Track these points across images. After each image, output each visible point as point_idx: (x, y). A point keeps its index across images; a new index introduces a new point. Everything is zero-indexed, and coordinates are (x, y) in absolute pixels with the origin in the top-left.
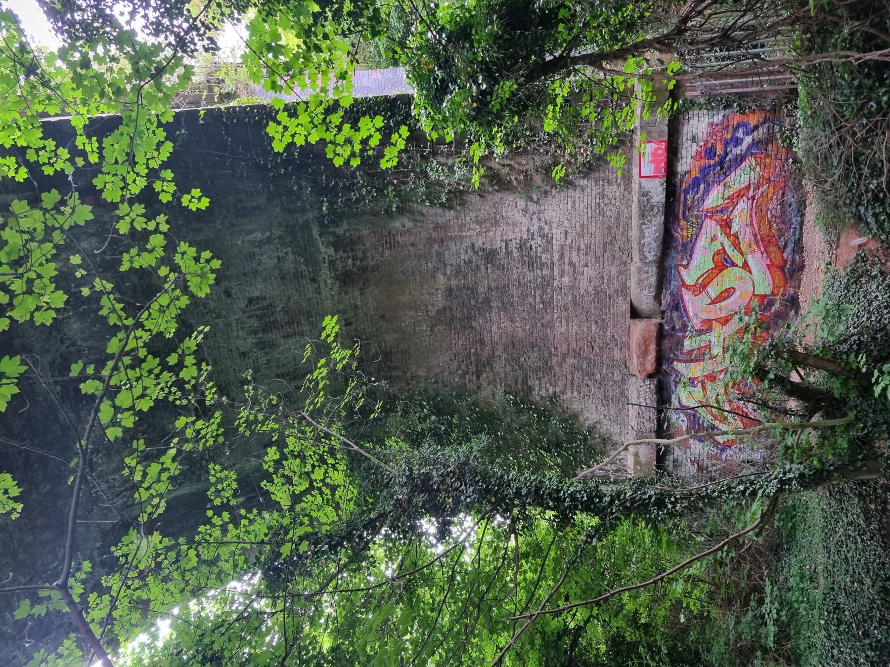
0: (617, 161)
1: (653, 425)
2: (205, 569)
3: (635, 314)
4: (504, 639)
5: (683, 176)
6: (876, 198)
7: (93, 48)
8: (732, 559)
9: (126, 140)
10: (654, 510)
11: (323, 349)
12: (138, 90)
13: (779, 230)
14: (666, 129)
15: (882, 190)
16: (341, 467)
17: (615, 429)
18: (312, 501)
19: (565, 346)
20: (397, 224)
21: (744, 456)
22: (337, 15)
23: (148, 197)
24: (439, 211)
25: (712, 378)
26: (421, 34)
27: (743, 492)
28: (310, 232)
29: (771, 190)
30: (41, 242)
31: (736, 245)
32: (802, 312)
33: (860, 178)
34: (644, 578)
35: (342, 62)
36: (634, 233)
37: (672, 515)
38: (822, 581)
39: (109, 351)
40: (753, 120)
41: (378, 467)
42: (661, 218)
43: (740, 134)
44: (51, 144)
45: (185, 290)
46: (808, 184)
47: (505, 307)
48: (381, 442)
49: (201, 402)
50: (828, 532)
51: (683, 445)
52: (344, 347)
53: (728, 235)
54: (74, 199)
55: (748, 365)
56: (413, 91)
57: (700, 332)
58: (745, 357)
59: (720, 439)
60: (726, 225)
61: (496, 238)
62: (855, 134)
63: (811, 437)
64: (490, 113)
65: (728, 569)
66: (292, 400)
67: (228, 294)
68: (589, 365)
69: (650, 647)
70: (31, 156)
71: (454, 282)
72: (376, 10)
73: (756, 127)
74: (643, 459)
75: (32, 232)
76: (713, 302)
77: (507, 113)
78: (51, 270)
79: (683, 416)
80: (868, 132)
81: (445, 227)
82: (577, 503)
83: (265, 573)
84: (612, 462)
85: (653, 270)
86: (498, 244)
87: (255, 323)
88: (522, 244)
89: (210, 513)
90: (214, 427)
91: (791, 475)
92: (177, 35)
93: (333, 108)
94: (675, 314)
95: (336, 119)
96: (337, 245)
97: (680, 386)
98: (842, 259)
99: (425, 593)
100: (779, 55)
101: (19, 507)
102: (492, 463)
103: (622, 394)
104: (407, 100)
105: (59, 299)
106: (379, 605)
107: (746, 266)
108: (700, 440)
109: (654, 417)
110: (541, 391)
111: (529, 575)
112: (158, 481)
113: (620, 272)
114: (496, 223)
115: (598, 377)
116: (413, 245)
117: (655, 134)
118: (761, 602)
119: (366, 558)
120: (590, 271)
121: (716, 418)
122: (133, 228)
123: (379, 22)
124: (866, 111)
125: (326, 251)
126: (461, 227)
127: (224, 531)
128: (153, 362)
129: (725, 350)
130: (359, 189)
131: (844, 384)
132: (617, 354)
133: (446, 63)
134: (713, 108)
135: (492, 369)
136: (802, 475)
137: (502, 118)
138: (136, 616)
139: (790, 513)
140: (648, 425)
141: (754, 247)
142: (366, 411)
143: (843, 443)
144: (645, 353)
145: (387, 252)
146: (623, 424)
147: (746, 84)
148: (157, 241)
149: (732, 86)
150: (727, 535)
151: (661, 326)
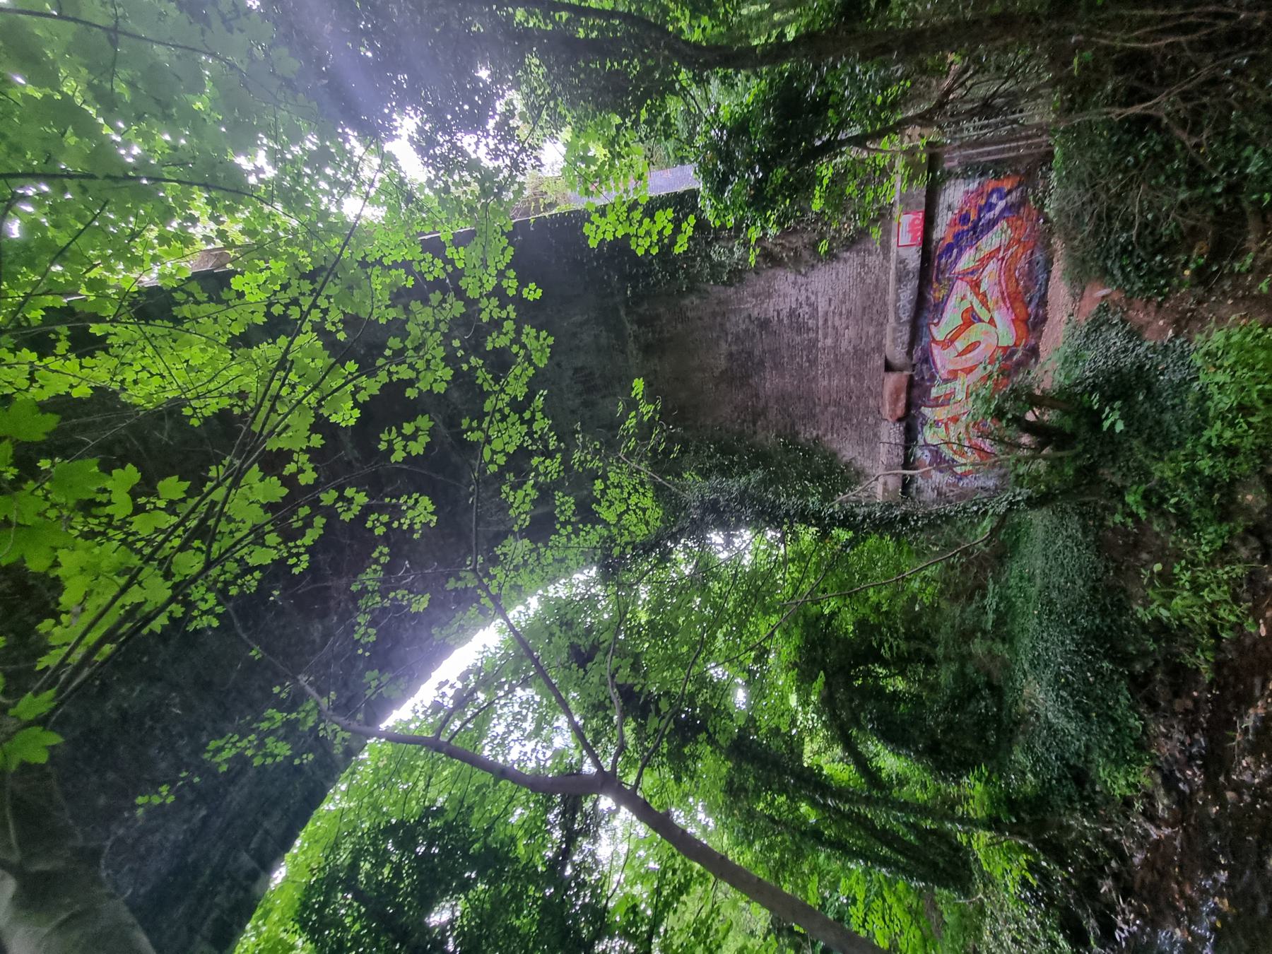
0: (876, 233)
1: (901, 460)
2: (557, 565)
3: (889, 367)
4: (774, 619)
5: (938, 243)
6: (1124, 250)
7: (451, 176)
8: (962, 564)
9: (480, 248)
10: (899, 526)
11: (632, 405)
12: (485, 206)
13: (1025, 287)
14: (923, 200)
15: (1131, 243)
16: (650, 494)
17: (868, 463)
18: (631, 518)
19: (827, 398)
20: (687, 302)
21: (980, 483)
22: (636, 123)
23: (499, 292)
24: (722, 288)
25: (955, 420)
26: (706, 132)
27: (977, 512)
28: (618, 311)
29: (1021, 250)
30: (432, 332)
31: (984, 303)
32: (1042, 360)
33: (1110, 233)
34: (887, 578)
35: (640, 164)
36: (891, 297)
37: (913, 530)
38: (1038, 581)
39: (486, 410)
40: (1007, 186)
41: (677, 495)
42: (915, 282)
43: (994, 199)
44: (429, 256)
45: (531, 363)
46: (1058, 243)
47: (777, 366)
48: (679, 476)
49: (546, 447)
50: (1048, 543)
51: (926, 476)
52: (648, 403)
53: (977, 294)
54: (451, 297)
55: (989, 408)
56: (699, 185)
57: (946, 381)
58: (987, 401)
59: (958, 470)
60: (976, 285)
61: (770, 308)
62: (1109, 190)
63: (1041, 466)
64: (764, 199)
65: (958, 572)
66: (611, 445)
67: (559, 365)
68: (847, 412)
69: (889, 628)
70: (416, 268)
71: (734, 348)
72: (668, 116)
73: (1010, 192)
74: (890, 488)
75: (426, 324)
76: (960, 355)
77: (779, 198)
78: (440, 352)
79: (927, 452)
80: (1123, 187)
81: (726, 302)
82: (835, 521)
83: (599, 568)
84: (864, 490)
85: (906, 330)
86: (771, 313)
87: (580, 387)
88: (792, 313)
89: (558, 526)
90: (557, 465)
91: (1019, 498)
92: (512, 158)
93: (633, 206)
94: (925, 367)
95: (637, 215)
96: (641, 322)
97: (926, 428)
98: (1085, 310)
99: (715, 586)
100: (1037, 118)
101: (435, 518)
102: (766, 490)
103: (875, 435)
104: (694, 194)
105: (448, 373)
106: (680, 593)
107: (992, 321)
108: (941, 471)
109: (901, 453)
110: (807, 434)
111: (796, 575)
112: (524, 502)
113: (876, 333)
114: (770, 296)
115: (855, 421)
116: (700, 318)
117: (913, 206)
118: (984, 596)
119: (670, 560)
120: (850, 333)
121: (955, 452)
122: (491, 317)
123: (670, 125)
124: (1122, 166)
125: (631, 328)
126: (740, 301)
127: (569, 539)
128: (514, 417)
129: (968, 396)
130: (656, 275)
131: (1076, 421)
132: (872, 402)
133: (727, 157)
134: (969, 177)
135: (766, 418)
136: (1029, 498)
137: (776, 202)
138: (514, 594)
139: (1016, 528)
140: (896, 460)
141: (1001, 303)
142: (667, 452)
143: (1069, 471)
144: (895, 401)
145: (679, 326)
146: (874, 460)
147: (1003, 151)
148: (509, 326)
149: (989, 153)
150: (958, 545)
151: (911, 377)
